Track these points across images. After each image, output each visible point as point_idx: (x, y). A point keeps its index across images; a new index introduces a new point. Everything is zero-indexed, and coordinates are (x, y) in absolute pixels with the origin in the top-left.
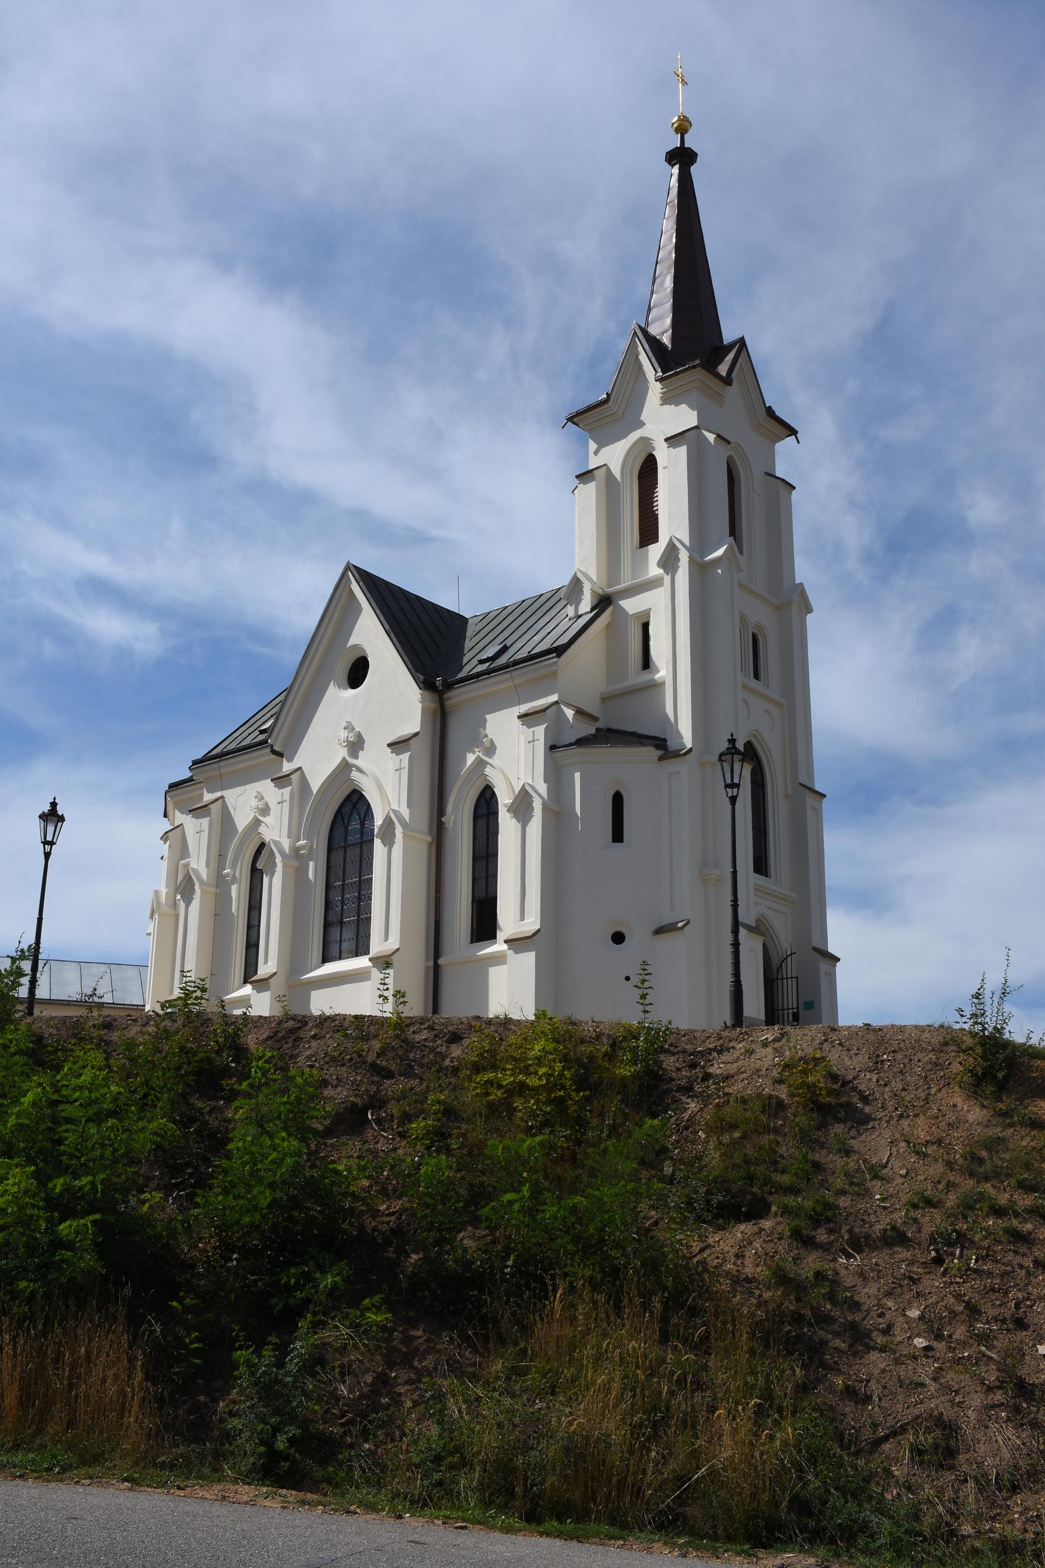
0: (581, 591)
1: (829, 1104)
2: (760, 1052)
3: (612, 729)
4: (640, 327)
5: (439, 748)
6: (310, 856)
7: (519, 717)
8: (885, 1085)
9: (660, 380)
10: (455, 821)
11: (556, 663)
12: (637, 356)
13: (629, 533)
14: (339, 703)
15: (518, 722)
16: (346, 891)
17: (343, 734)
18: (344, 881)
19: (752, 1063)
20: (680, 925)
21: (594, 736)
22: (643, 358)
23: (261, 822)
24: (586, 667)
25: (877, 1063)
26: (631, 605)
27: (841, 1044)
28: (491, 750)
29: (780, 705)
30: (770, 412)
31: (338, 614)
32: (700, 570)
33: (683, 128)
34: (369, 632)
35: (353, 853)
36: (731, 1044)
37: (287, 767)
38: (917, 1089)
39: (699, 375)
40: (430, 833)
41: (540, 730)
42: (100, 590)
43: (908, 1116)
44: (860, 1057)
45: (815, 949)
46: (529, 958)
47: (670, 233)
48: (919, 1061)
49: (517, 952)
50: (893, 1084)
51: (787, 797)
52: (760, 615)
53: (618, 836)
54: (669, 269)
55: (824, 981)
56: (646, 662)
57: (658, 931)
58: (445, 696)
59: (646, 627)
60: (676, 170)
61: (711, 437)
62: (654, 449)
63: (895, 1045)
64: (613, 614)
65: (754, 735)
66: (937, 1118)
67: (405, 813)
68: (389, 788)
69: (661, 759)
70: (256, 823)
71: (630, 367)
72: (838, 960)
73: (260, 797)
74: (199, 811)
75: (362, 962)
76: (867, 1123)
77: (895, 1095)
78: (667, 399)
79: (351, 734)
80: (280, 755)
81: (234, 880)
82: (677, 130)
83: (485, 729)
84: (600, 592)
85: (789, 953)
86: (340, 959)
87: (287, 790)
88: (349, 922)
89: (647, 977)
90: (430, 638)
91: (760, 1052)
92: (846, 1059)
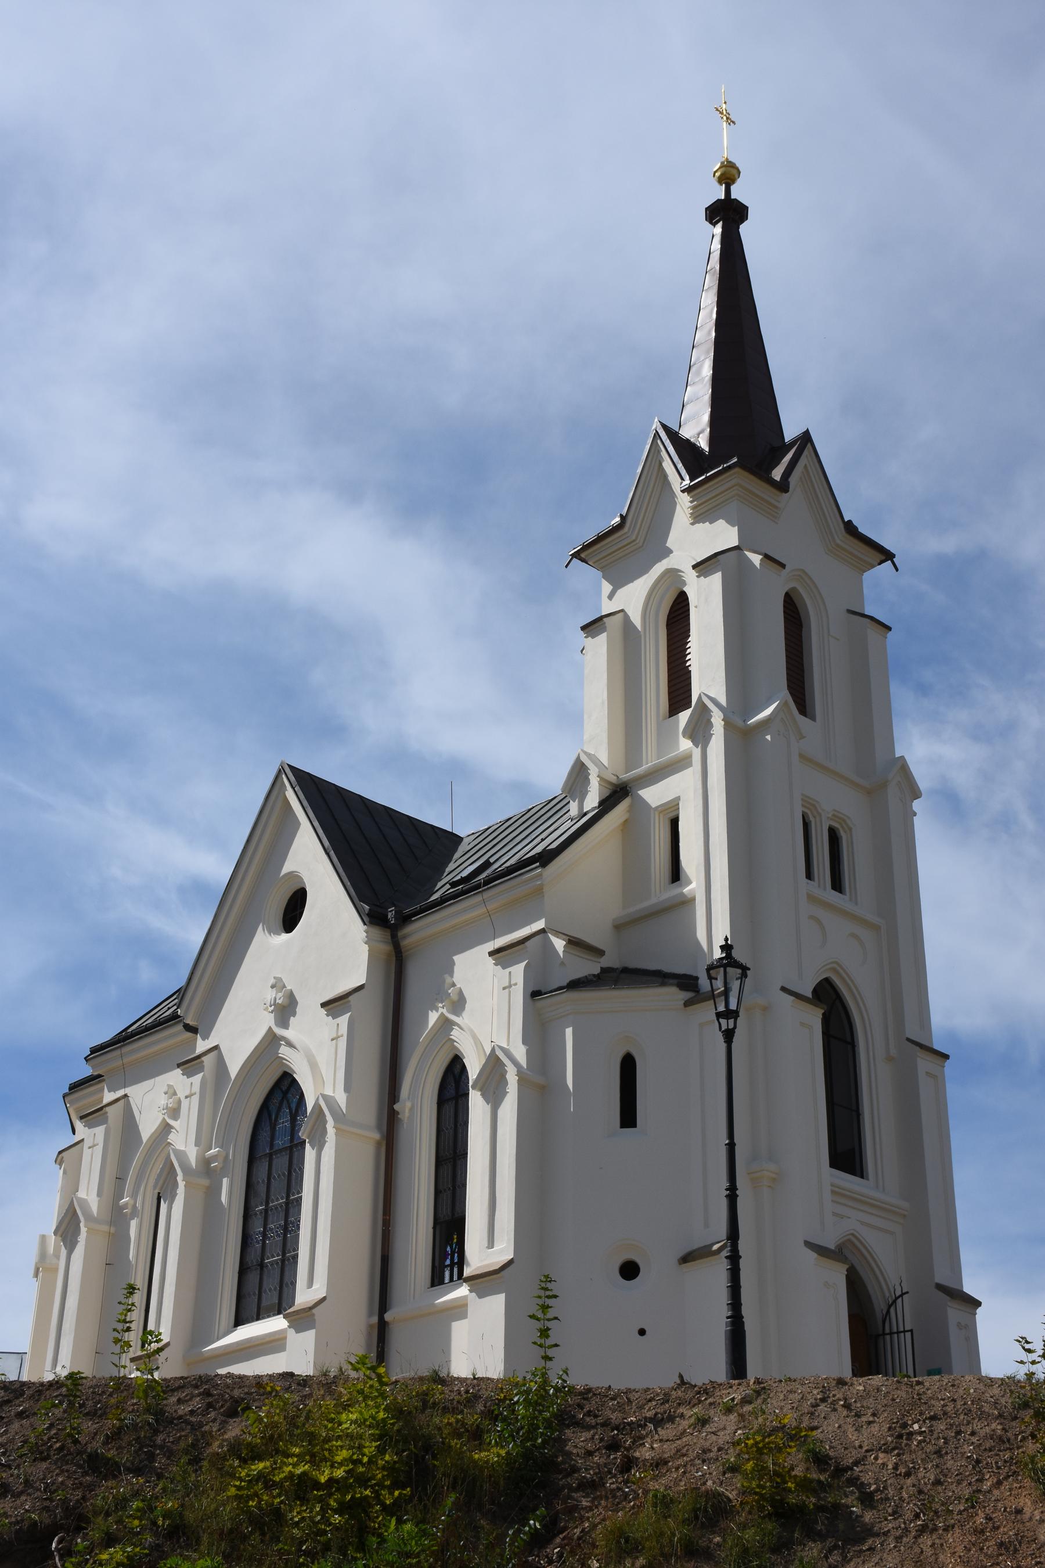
0: (586, 781)
1: (801, 1508)
2: (718, 1419)
3: (619, 967)
4: (665, 427)
5: (394, 1005)
6: (223, 1171)
7: (491, 954)
8: (908, 1474)
9: (688, 490)
10: (411, 1109)
11: (540, 875)
12: (661, 464)
13: (654, 702)
14: (269, 953)
15: (491, 961)
16: (270, 1219)
17: (270, 995)
18: (267, 1203)
19: (701, 1439)
20: (715, 1247)
22: (667, 465)
23: (171, 1127)
24: (589, 882)
25: (900, 1436)
26: (654, 795)
27: (847, 1406)
28: (459, 1004)
29: (876, 928)
30: (850, 528)
31: (268, 835)
32: (742, 740)
33: (728, 175)
34: (309, 858)
35: (281, 1163)
36: (681, 1410)
37: (202, 1045)
38: (959, 1483)
39: (739, 479)
40: (379, 1127)
41: (518, 971)
43: (935, 1529)
44: (875, 1429)
45: (940, 1287)
46: (497, 1303)
47: (710, 307)
48: (973, 1434)
49: (481, 1295)
50: (921, 1473)
51: (890, 1059)
52: (837, 802)
53: (628, 1118)
54: (708, 352)
55: (955, 1337)
56: (676, 873)
57: (686, 1259)
58: (400, 934)
59: (675, 823)
60: (718, 230)
61: (756, 559)
62: (684, 583)
63: (937, 1407)
64: (631, 809)
65: (834, 970)
66: (982, 1532)
67: (341, 1098)
68: (324, 1063)
69: (687, 1004)
70: (166, 1129)
71: (653, 476)
72: (978, 1304)
73: (171, 1092)
74: (93, 1116)
75: (276, 1324)
76: (862, 1540)
77: (920, 1492)
78: (699, 516)
79: (280, 995)
80: (194, 1030)
81: (134, 1213)
82: (720, 181)
83: (452, 976)
84: (613, 779)
85: (898, 1293)
86: (258, 1319)
87: (197, 1079)
88: (272, 1263)
89: (550, 1302)
90: (396, 865)
91: (718, 1419)
92: (851, 1430)
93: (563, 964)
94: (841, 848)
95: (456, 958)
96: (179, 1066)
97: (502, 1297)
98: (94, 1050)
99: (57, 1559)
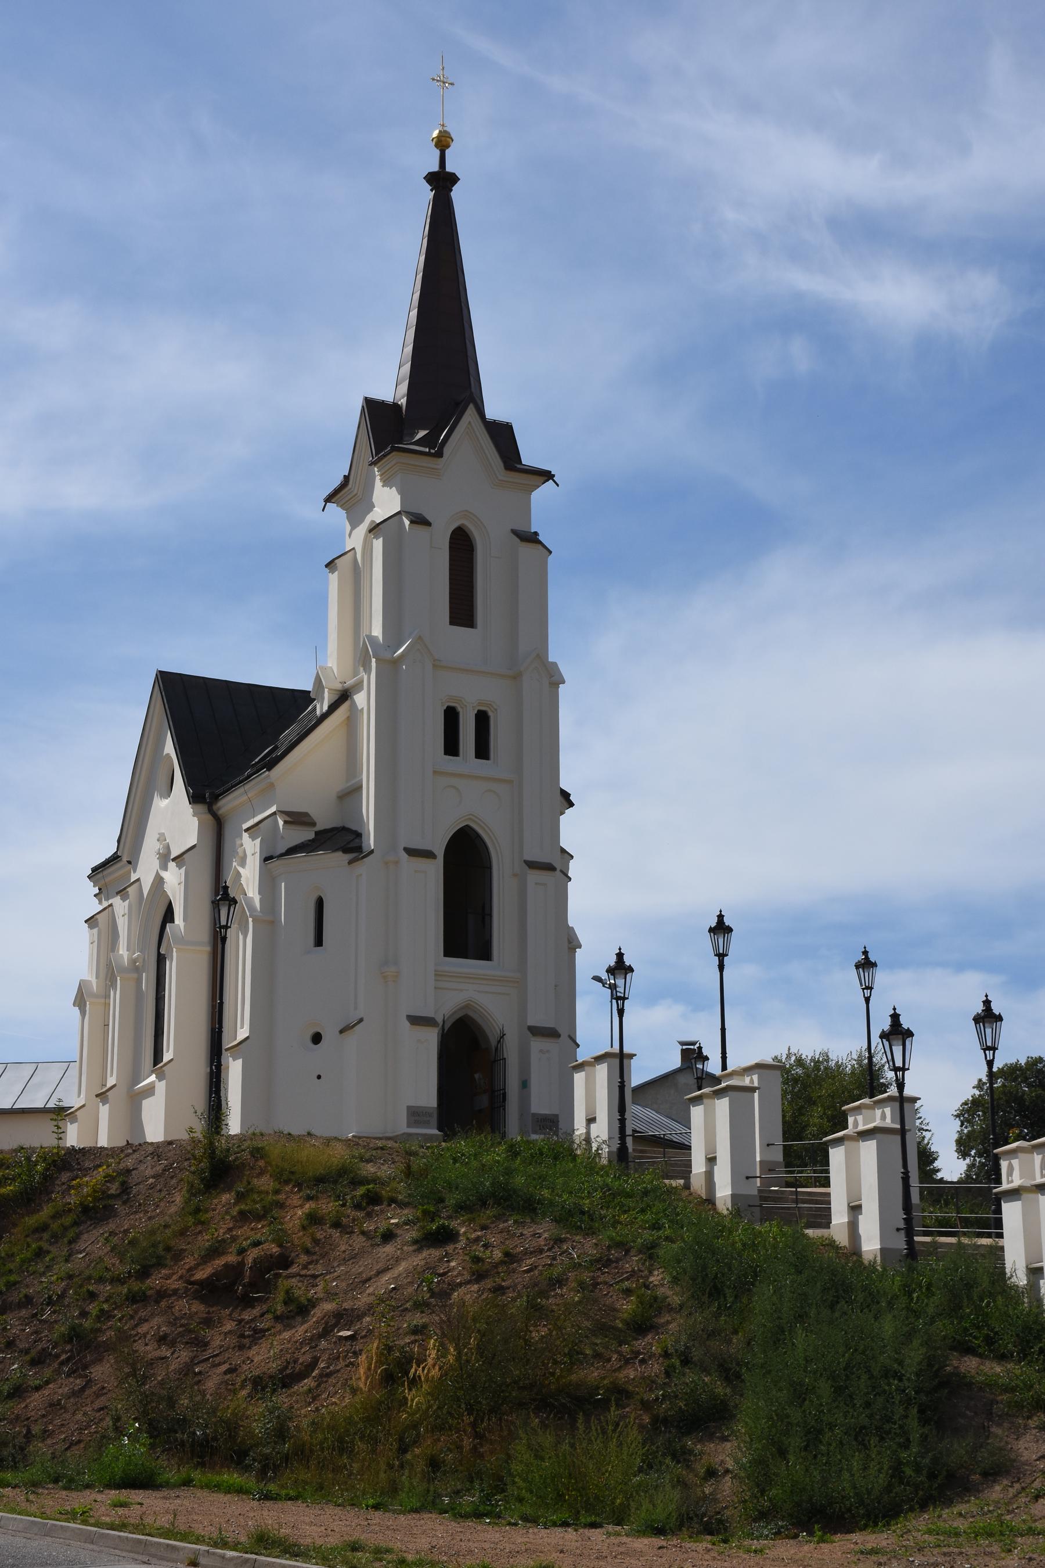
21: (313, 841)
42: (870, 232)
53: (319, 942)
69: (350, 862)
93: (282, 837)
94: (489, 726)
95: (550, 660)
96: (118, 893)
97: (241, 1060)
98: (94, 870)
99: (758, 1159)
